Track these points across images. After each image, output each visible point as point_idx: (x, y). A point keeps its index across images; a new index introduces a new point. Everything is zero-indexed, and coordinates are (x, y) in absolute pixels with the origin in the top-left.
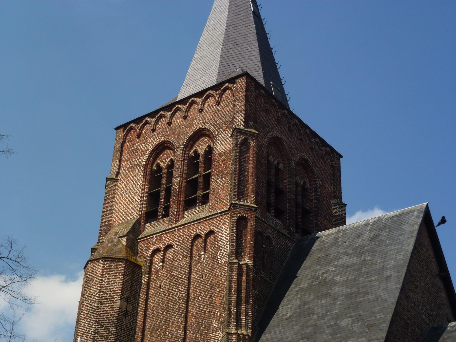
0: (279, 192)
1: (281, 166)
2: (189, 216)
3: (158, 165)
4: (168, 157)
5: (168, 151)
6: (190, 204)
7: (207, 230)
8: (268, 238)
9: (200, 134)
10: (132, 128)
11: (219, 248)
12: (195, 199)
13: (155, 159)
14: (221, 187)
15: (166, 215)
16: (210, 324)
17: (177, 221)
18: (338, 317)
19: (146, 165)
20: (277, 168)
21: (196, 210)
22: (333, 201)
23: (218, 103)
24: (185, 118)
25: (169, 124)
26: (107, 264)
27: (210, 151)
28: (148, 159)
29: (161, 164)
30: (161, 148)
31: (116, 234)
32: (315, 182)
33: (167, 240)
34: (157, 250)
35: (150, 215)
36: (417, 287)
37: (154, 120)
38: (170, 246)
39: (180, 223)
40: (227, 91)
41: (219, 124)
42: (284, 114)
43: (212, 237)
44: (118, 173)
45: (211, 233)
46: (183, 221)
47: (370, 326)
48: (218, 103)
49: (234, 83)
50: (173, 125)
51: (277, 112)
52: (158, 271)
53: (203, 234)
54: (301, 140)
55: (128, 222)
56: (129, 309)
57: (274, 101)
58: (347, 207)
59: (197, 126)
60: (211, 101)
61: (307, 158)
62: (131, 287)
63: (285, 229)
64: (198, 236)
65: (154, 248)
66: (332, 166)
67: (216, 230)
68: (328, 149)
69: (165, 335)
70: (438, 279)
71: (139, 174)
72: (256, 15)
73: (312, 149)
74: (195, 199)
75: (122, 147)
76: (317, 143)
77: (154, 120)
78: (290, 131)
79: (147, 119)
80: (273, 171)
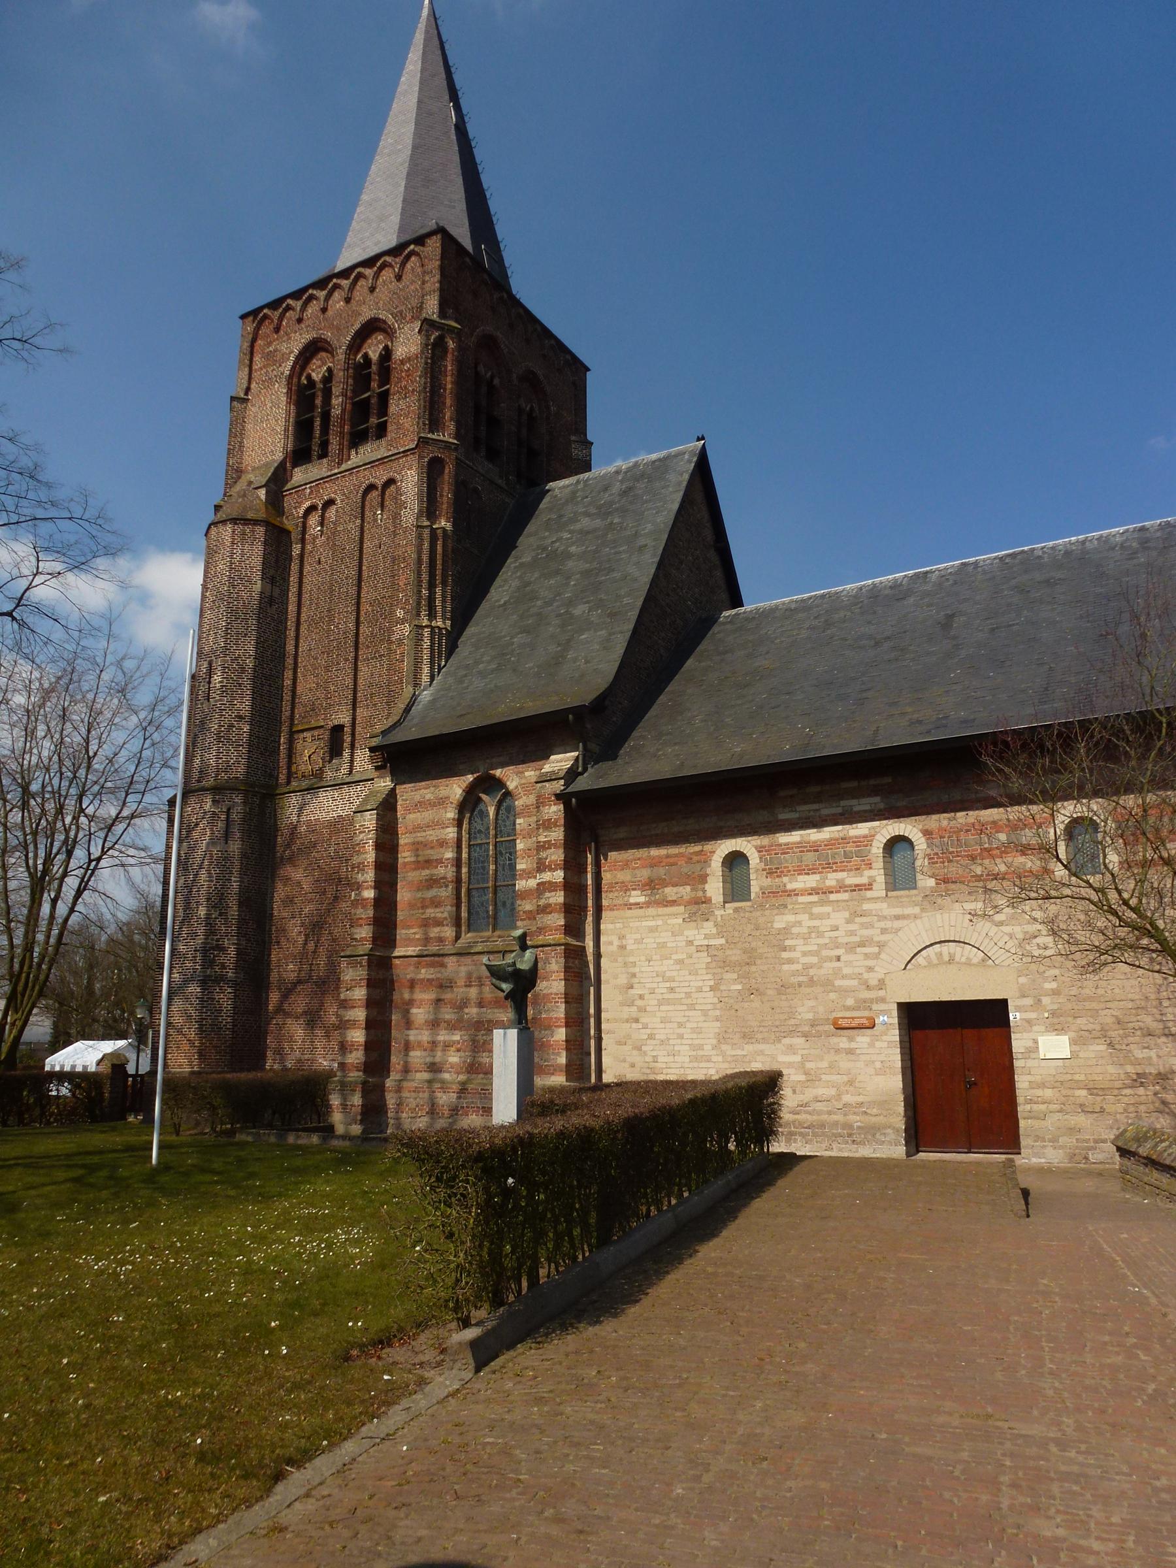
1: (496, 381)
3: (309, 377)
4: (324, 364)
5: (324, 354)
8: (475, 490)
9: (372, 327)
10: (266, 317)
11: (403, 505)
14: (405, 410)
15: (323, 455)
16: (392, 613)
17: (340, 464)
18: (570, 603)
19: (290, 377)
23: (399, 278)
24: (348, 300)
25: (324, 310)
26: (239, 528)
28: (293, 367)
29: (314, 375)
34: (312, 509)
35: (300, 455)
38: (331, 502)
39: (344, 467)
40: (413, 258)
41: (401, 312)
43: (393, 488)
44: (248, 390)
45: (391, 482)
47: (612, 615)
48: (399, 278)
50: (330, 313)
53: (379, 483)
55: (267, 465)
59: (367, 314)
60: (387, 274)
62: (277, 561)
65: (307, 504)
69: (329, 630)
71: (280, 391)
75: (252, 346)
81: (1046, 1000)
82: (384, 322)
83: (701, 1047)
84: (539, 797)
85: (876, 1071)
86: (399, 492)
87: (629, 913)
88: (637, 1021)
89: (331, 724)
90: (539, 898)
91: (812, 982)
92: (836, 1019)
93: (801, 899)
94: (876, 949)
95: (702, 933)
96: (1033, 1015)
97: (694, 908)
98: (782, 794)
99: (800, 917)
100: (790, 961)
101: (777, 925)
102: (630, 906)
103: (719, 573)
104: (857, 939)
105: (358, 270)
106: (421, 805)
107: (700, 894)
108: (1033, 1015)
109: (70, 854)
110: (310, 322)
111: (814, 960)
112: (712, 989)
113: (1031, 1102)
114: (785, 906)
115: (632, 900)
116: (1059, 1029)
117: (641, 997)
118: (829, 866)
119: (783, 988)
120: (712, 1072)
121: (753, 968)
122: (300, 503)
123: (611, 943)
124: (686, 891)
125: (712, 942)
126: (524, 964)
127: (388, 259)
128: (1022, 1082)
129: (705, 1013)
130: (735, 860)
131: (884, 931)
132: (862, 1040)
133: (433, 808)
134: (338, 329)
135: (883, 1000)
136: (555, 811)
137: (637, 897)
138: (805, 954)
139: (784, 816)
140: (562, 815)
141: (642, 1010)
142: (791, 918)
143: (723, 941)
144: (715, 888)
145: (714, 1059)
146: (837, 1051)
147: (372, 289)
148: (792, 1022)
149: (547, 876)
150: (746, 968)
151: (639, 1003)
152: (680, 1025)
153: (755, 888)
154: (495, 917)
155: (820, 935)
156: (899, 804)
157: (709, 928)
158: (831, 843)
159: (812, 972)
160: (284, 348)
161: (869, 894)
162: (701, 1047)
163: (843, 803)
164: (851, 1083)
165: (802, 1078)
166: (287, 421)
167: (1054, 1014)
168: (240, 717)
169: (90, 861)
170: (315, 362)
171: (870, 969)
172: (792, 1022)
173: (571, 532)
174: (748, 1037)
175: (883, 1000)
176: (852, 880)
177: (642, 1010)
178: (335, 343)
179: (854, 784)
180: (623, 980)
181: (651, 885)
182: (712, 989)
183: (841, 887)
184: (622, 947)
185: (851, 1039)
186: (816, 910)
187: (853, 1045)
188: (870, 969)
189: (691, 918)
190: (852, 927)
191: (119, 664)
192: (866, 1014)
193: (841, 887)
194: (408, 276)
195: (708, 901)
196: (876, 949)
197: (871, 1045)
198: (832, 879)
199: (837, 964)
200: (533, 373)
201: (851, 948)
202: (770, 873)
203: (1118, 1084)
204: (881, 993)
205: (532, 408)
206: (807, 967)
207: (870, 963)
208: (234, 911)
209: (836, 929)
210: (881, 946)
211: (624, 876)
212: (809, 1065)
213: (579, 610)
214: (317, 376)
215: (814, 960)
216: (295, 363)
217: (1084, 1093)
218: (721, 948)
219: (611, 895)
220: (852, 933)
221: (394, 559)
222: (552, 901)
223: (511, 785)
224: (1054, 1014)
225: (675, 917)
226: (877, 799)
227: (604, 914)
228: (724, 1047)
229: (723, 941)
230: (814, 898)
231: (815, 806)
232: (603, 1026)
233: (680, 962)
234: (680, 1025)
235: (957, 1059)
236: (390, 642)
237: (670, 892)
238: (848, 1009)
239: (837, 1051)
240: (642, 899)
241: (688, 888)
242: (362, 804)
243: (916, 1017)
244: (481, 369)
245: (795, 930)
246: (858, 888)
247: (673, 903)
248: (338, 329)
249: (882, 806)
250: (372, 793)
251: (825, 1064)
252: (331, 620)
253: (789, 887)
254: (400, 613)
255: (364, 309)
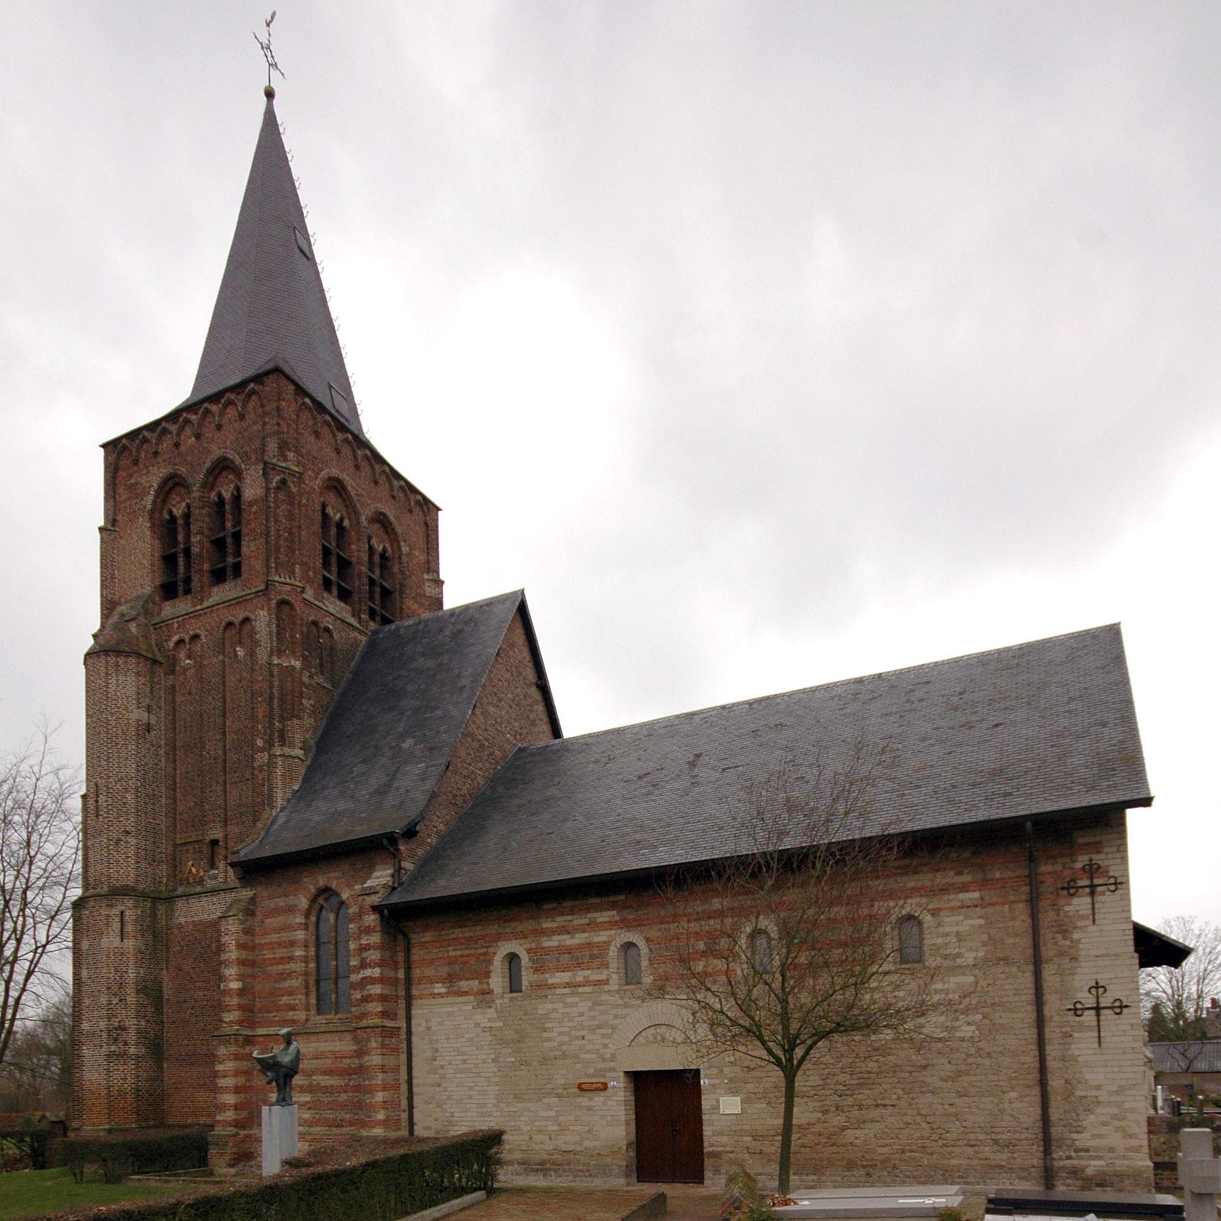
0: (344, 564)
1: (346, 523)
2: (221, 593)
3: (171, 513)
4: (183, 500)
5: (182, 490)
6: (219, 576)
7: (241, 617)
8: (327, 630)
9: (222, 467)
10: (125, 447)
11: (257, 644)
12: (224, 569)
13: (164, 502)
15: (188, 591)
16: (253, 743)
17: (202, 601)
18: (402, 737)
19: (152, 511)
20: (339, 525)
21: (227, 586)
22: (426, 576)
23: (242, 417)
24: (198, 436)
25: (177, 445)
26: (112, 660)
27: (237, 498)
28: (154, 502)
29: (174, 510)
30: (170, 484)
31: (123, 615)
32: (399, 547)
33: (194, 627)
34: (181, 641)
35: (169, 591)
36: (500, 700)
37: (242, 397)
39: (206, 604)
40: (254, 397)
41: (246, 453)
42: (346, 440)
45: (246, 620)
46: (211, 601)
47: (432, 749)
48: (242, 417)
49: (262, 384)
50: (183, 448)
51: (335, 436)
52: (185, 670)
53: (237, 621)
54: (376, 483)
55: (138, 598)
56: (153, 722)
57: (328, 418)
58: (445, 587)
59: (217, 453)
60: (231, 413)
61: (386, 511)
62: (152, 691)
63: (353, 616)
64: (230, 624)
65: (175, 638)
66: (426, 524)
67: (253, 617)
68: (419, 497)
69: (201, 756)
70: (534, 688)
71: (144, 523)
72: (270, 127)
73: (394, 497)
74: (224, 569)
76: (402, 488)
77: (156, 435)
78: (357, 467)
79: (206, 405)
80: (333, 531)
81: (726, 1070)
82: (233, 462)
83: (485, 1105)
84: (361, 907)
85: (611, 1122)
86: (253, 632)
87: (433, 1001)
88: (439, 1085)
89: (208, 839)
90: (362, 990)
91: (564, 1056)
92: (580, 1084)
93: (558, 991)
94: (609, 1031)
95: (486, 1017)
96: (717, 1081)
97: (481, 997)
98: (546, 906)
99: (556, 1006)
100: (549, 1040)
101: (540, 1012)
102: (434, 996)
103: (540, 708)
104: (596, 1023)
105: (228, 395)
106: (276, 912)
107: (485, 986)
108: (717, 1081)
109: (19, 941)
110: (166, 457)
111: (566, 1039)
112: (494, 1061)
113: (713, 1145)
114: (546, 996)
115: (436, 991)
116: (734, 1092)
117: (442, 1067)
118: (579, 966)
119: (544, 1061)
120: (493, 1124)
121: (523, 1045)
122: (170, 637)
123: (420, 1025)
124: (475, 984)
125: (493, 1025)
126: (286, 1059)
127: (232, 396)
128: (707, 1131)
129: (488, 1079)
130: (512, 958)
131: (616, 1017)
132: (599, 1099)
133: (288, 911)
134: (191, 465)
135: (614, 1070)
136: (371, 919)
137: (439, 988)
138: (560, 1034)
139: (547, 924)
140: (378, 922)
141: (443, 1077)
142: (550, 1006)
143: (501, 1024)
144: (497, 981)
145: (495, 1114)
146: (581, 1108)
147: (219, 427)
148: (550, 1086)
149: (368, 972)
150: (518, 1045)
151: (441, 1071)
152: (470, 1088)
153: (525, 983)
154: (337, 1003)
155: (571, 1020)
156: (630, 917)
157: (491, 1013)
158: (580, 947)
159: (564, 1048)
160: (144, 480)
161: (606, 988)
162: (485, 1105)
163: (590, 915)
164: (590, 1131)
165: (556, 1128)
166: (152, 555)
167: (731, 1080)
168: (127, 832)
169: (37, 948)
170: (175, 498)
171: (606, 1046)
172: (550, 1086)
173: (409, 670)
174: (518, 1097)
175: (614, 1070)
176: (595, 976)
177: (443, 1077)
178: (190, 480)
179: (597, 900)
180: (429, 1054)
181: (450, 979)
182: (494, 1061)
183: (586, 983)
184: (429, 1028)
185: (591, 1099)
186: (568, 1000)
187: (592, 1103)
188: (606, 1046)
189: (479, 1005)
190: (592, 1014)
191: (56, 772)
192: (602, 1080)
193: (586, 983)
194: (251, 417)
195: (490, 992)
196: (609, 1031)
197: (605, 1103)
198: (580, 976)
199: (582, 1042)
200: (384, 514)
201: (593, 1030)
202: (536, 970)
203: (772, 1133)
204: (613, 1064)
205: (385, 549)
206: (561, 1044)
207: (607, 1041)
208: (131, 999)
209: (582, 1014)
210: (614, 1028)
211: (429, 972)
212: (561, 1119)
213: (407, 744)
214: (178, 512)
215: (566, 1039)
216: (157, 496)
217: (749, 1139)
218: (500, 1029)
219: (421, 987)
220: (594, 1018)
221: (253, 694)
222: (372, 992)
223: (344, 896)
224: (731, 1080)
225: (466, 1005)
226: (614, 913)
227: (414, 1002)
228: (502, 1105)
229: (501, 1024)
230: (567, 990)
231: (569, 918)
232: (415, 1090)
233: (471, 1040)
234: (470, 1088)
235: (665, 1110)
236: (253, 768)
237: (464, 985)
238: (589, 1076)
239: (581, 1108)
240: (443, 990)
241: (477, 982)
242: (227, 911)
243: (641, 1081)
244: (329, 510)
245: (553, 1015)
246: (598, 983)
247: (466, 993)
248: (191, 465)
249: (617, 918)
250: (235, 902)
251: (572, 1118)
252: (203, 747)
253: (550, 982)
254: (260, 743)
255: (213, 447)
